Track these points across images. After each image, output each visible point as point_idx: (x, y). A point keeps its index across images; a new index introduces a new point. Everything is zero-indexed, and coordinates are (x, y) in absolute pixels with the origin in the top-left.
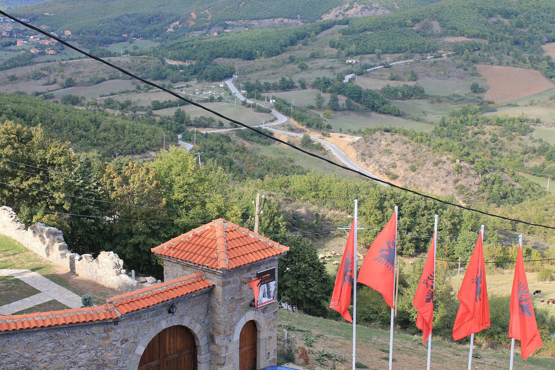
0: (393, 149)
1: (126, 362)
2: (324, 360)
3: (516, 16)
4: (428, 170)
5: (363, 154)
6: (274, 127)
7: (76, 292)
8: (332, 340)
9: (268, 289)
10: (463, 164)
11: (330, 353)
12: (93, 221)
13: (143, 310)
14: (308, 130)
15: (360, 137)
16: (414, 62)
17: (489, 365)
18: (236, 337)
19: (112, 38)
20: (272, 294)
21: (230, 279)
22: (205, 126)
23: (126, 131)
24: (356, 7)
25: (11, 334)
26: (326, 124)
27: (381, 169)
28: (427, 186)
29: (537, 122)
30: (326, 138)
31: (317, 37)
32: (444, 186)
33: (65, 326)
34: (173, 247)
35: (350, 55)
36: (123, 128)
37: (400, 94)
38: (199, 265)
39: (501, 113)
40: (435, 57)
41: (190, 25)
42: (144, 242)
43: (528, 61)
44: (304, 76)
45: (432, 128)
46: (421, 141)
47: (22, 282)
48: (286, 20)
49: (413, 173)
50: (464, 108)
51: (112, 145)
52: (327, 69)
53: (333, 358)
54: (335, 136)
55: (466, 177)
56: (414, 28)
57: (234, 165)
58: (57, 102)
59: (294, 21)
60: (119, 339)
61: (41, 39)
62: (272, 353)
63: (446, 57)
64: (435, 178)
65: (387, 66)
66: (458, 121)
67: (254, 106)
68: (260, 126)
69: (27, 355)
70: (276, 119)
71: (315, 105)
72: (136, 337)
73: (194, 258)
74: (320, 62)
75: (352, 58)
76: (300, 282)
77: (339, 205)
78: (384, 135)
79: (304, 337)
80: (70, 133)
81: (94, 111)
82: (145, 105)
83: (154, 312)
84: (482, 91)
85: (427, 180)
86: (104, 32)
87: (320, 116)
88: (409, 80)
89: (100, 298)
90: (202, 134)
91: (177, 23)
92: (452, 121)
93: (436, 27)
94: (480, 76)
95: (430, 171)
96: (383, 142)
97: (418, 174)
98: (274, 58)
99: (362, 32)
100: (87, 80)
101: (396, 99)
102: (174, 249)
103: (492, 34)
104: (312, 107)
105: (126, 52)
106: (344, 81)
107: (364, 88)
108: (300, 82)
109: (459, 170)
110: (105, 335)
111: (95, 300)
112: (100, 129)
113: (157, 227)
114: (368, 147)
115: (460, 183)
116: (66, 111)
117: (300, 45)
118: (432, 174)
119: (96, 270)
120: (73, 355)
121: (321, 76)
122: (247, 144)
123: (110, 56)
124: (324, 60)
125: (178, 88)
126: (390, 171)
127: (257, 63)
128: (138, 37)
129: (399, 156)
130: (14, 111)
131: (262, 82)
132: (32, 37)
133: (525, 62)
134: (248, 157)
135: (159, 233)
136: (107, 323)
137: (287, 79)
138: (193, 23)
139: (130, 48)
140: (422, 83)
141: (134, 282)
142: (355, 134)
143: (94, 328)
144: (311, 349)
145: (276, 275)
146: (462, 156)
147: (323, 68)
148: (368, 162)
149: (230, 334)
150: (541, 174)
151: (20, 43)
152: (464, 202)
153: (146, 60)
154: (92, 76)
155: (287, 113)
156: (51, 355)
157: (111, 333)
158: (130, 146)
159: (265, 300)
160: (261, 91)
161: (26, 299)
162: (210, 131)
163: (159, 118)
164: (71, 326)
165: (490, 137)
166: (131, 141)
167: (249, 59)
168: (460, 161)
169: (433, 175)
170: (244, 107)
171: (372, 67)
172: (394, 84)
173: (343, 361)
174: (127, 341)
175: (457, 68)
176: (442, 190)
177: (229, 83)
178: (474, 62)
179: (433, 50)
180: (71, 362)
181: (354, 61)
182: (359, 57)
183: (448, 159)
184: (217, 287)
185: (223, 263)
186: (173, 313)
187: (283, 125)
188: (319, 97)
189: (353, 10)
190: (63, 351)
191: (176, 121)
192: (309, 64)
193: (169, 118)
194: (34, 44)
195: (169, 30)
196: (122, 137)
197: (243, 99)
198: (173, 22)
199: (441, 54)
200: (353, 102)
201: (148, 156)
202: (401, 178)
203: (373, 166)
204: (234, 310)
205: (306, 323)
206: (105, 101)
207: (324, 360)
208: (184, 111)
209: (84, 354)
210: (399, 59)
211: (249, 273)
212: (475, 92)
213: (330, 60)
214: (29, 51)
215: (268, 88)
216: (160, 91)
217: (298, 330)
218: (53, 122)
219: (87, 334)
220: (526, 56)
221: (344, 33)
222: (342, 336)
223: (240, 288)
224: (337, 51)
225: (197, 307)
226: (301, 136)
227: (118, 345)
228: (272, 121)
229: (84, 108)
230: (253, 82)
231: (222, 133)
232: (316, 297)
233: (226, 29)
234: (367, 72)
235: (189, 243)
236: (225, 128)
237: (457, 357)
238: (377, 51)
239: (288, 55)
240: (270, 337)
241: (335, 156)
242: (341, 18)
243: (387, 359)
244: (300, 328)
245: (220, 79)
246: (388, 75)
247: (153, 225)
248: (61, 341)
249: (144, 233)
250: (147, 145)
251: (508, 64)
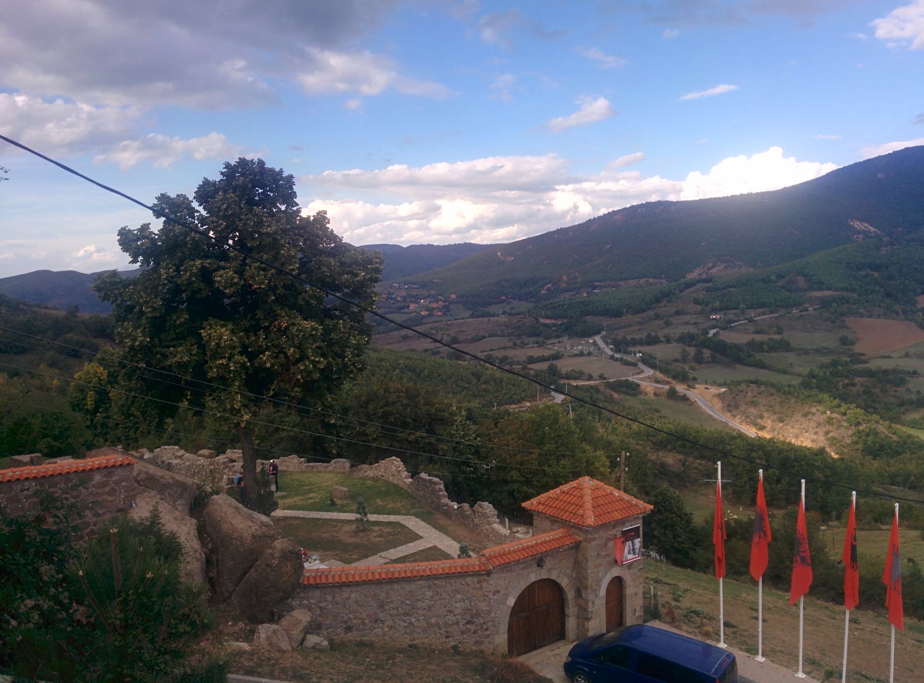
0: (760, 400)
1: (498, 613)
2: (691, 617)
3: (887, 268)
4: (797, 421)
5: (729, 406)
6: (641, 379)
7: (454, 539)
8: (699, 595)
9: (633, 546)
10: (834, 415)
11: (697, 609)
12: (472, 469)
13: (514, 563)
14: (674, 382)
15: (726, 389)
16: (779, 316)
17: (869, 632)
18: (603, 592)
19: (492, 300)
20: (637, 551)
21: (596, 536)
22: (576, 379)
23: (504, 384)
24: (720, 266)
25: (394, 582)
26: (691, 376)
27: (748, 420)
28: (797, 437)
29: (913, 374)
30: (692, 390)
31: (682, 294)
32: (814, 437)
33: (442, 576)
34: (542, 502)
35: (714, 311)
36: (501, 380)
37: (765, 347)
38: (566, 521)
39: (873, 365)
40: (801, 311)
41: (562, 287)
42: (518, 489)
43: (901, 313)
44: (667, 331)
45: (800, 380)
46: (789, 393)
47: (407, 527)
48: (651, 280)
49: (781, 424)
50: (833, 360)
51: (492, 396)
52: (691, 324)
53: (701, 615)
54: (700, 387)
55: (837, 429)
56: (779, 284)
57: (603, 415)
58: (443, 358)
59: (659, 280)
60: (491, 591)
61: (430, 302)
62: (638, 609)
63: (812, 311)
64: (804, 429)
65: (751, 320)
66: (828, 373)
67: (621, 359)
68: (628, 378)
69: (408, 602)
70: (642, 371)
71: (680, 358)
72: (507, 588)
73: (561, 514)
74: (685, 318)
75: (716, 314)
76: (667, 532)
77: (706, 454)
78: (750, 386)
79: (671, 591)
80: (454, 385)
81: (476, 366)
82: (521, 360)
83: (523, 565)
84: (852, 343)
85: (796, 431)
87: (685, 369)
88: (775, 333)
89: (476, 545)
90: (573, 386)
91: (550, 285)
92: (821, 373)
93: (801, 282)
94: (850, 328)
95: (799, 423)
96: (749, 394)
97: (787, 425)
98: (640, 315)
99: (726, 288)
100: (469, 337)
101: (762, 351)
102: (543, 504)
103: (861, 287)
104: (676, 360)
105: (504, 313)
106: (709, 336)
107: (728, 341)
108: (665, 337)
109: (830, 421)
110: (478, 586)
111: (471, 547)
112: (480, 382)
113: (530, 476)
114: (734, 398)
115: (831, 434)
116: (451, 366)
117: (664, 303)
118: (801, 424)
119: (473, 519)
120: (449, 603)
121: (686, 331)
122: (616, 396)
123: (490, 316)
124: (689, 316)
125: (551, 344)
126: (758, 422)
127: (624, 320)
128: (514, 299)
129: (766, 407)
130: (406, 366)
131: (629, 337)
132: (422, 301)
133: (897, 313)
134: (616, 408)
135: (532, 481)
136: (481, 575)
137: (653, 334)
138: (564, 285)
139: (507, 309)
140: (787, 336)
142: (721, 385)
143: (469, 579)
144: (678, 604)
145: (641, 532)
146: (833, 408)
147: (687, 323)
148: (734, 413)
149: (596, 590)
150: (921, 427)
151: (412, 306)
152: (837, 453)
153: (522, 319)
154: (474, 334)
155: (653, 366)
156: (429, 603)
157: (484, 585)
158: (507, 397)
159: (630, 556)
160: (628, 346)
161: (411, 544)
162: (580, 383)
163: (534, 372)
164: (448, 576)
165: (862, 389)
166: (508, 393)
167: (616, 316)
168: (831, 413)
169: (803, 426)
170: (611, 361)
171: (736, 321)
172: (758, 338)
173: (711, 619)
174: (498, 592)
175: (825, 321)
176: (813, 441)
177: (598, 338)
178: (843, 314)
179: (796, 305)
180: (447, 611)
181: (718, 317)
182: (723, 312)
183: (818, 410)
184: (583, 542)
185: (591, 520)
186: (542, 566)
187: (649, 377)
188: (684, 351)
189: (717, 268)
190: (440, 599)
191: (549, 374)
192: (673, 320)
193: (542, 371)
195: (543, 292)
196: (500, 389)
197: (611, 353)
198: (546, 284)
199: (807, 308)
200: (717, 355)
201: (523, 406)
202: (768, 428)
203: (739, 416)
204: (600, 565)
205: (674, 576)
206: (485, 356)
207: (691, 617)
208: (555, 366)
209: (459, 603)
210: (764, 314)
211: (614, 531)
212: (845, 344)
213: (695, 316)
215: (634, 343)
216: (534, 347)
217: (666, 583)
218: (439, 375)
219: (462, 584)
220: (898, 308)
221: (708, 290)
222: (711, 591)
223: (606, 544)
224: (700, 307)
225: (565, 561)
226: (667, 387)
227: (491, 596)
228: (639, 374)
229: (467, 363)
230: (620, 337)
231: (592, 385)
232: (684, 547)
233: (594, 289)
234: (731, 327)
235: (557, 499)
236: (595, 380)
237: (834, 621)
238: (742, 306)
239: (654, 313)
240: (636, 594)
241: (701, 407)
242: (704, 276)
243: (757, 619)
244: (667, 581)
245: (590, 335)
246: (753, 329)
247: (527, 474)
248: (438, 590)
249: (518, 481)
250: (523, 396)
251: (879, 316)
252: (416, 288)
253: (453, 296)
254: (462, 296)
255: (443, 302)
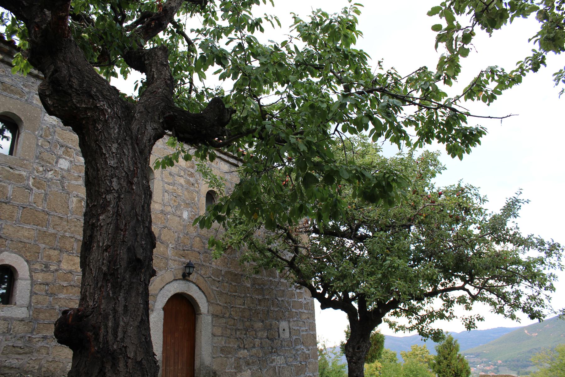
61: (484, 366)
86: (523, 360)
132: (478, 366)
141: (228, 177)
194: (480, 370)
214: (478, 374)
252: (473, 357)
253: (500, 362)
254: (506, 361)
255: (493, 365)
